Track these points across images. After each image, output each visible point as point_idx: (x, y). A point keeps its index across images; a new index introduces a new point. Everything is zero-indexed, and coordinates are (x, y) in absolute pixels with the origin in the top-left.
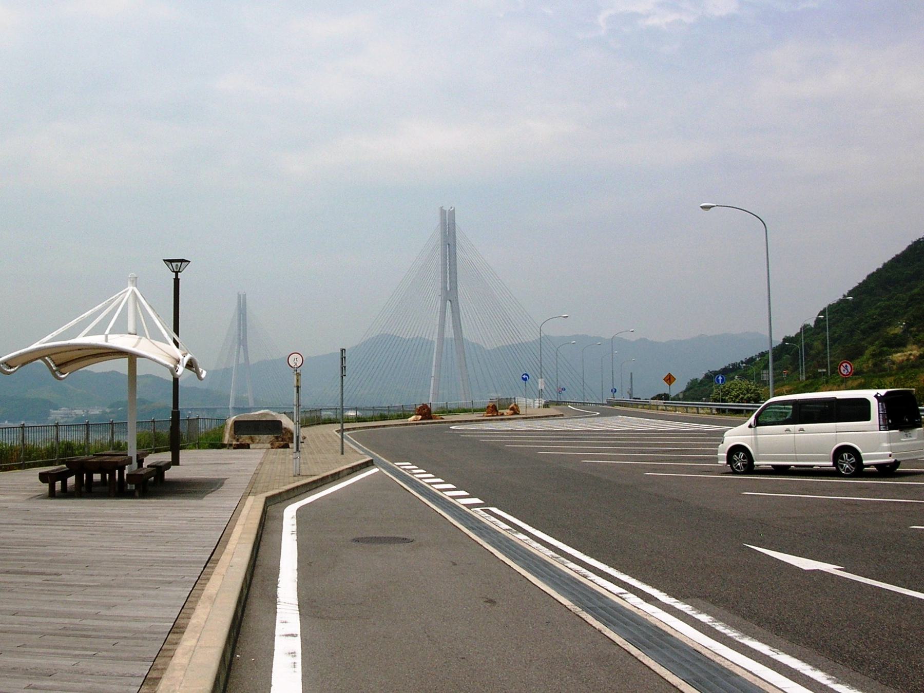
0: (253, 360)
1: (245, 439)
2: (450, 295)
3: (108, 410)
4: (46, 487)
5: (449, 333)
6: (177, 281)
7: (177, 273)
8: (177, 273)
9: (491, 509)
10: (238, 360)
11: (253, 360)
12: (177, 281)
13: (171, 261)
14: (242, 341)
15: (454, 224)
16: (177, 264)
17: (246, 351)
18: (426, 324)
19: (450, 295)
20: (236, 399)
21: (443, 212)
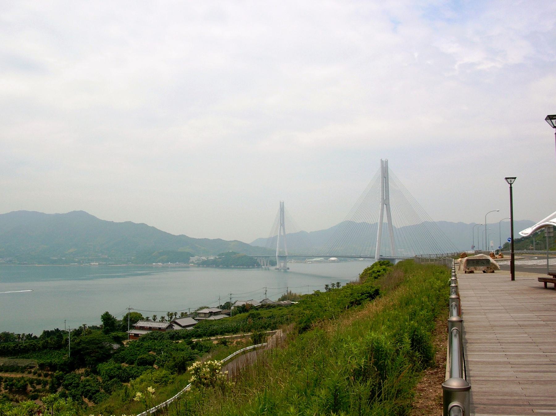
0: (287, 233)
1: (472, 268)
2: (386, 202)
3: (217, 257)
4: (542, 284)
5: (385, 220)
6: (511, 188)
7: (511, 184)
8: (511, 184)
9: (149, 332)
10: (280, 233)
11: (287, 233)
12: (511, 188)
13: (508, 178)
14: (282, 224)
15: (387, 167)
16: (510, 180)
17: (284, 229)
18: (373, 216)
19: (386, 202)
20: (280, 252)
21: (382, 161)
